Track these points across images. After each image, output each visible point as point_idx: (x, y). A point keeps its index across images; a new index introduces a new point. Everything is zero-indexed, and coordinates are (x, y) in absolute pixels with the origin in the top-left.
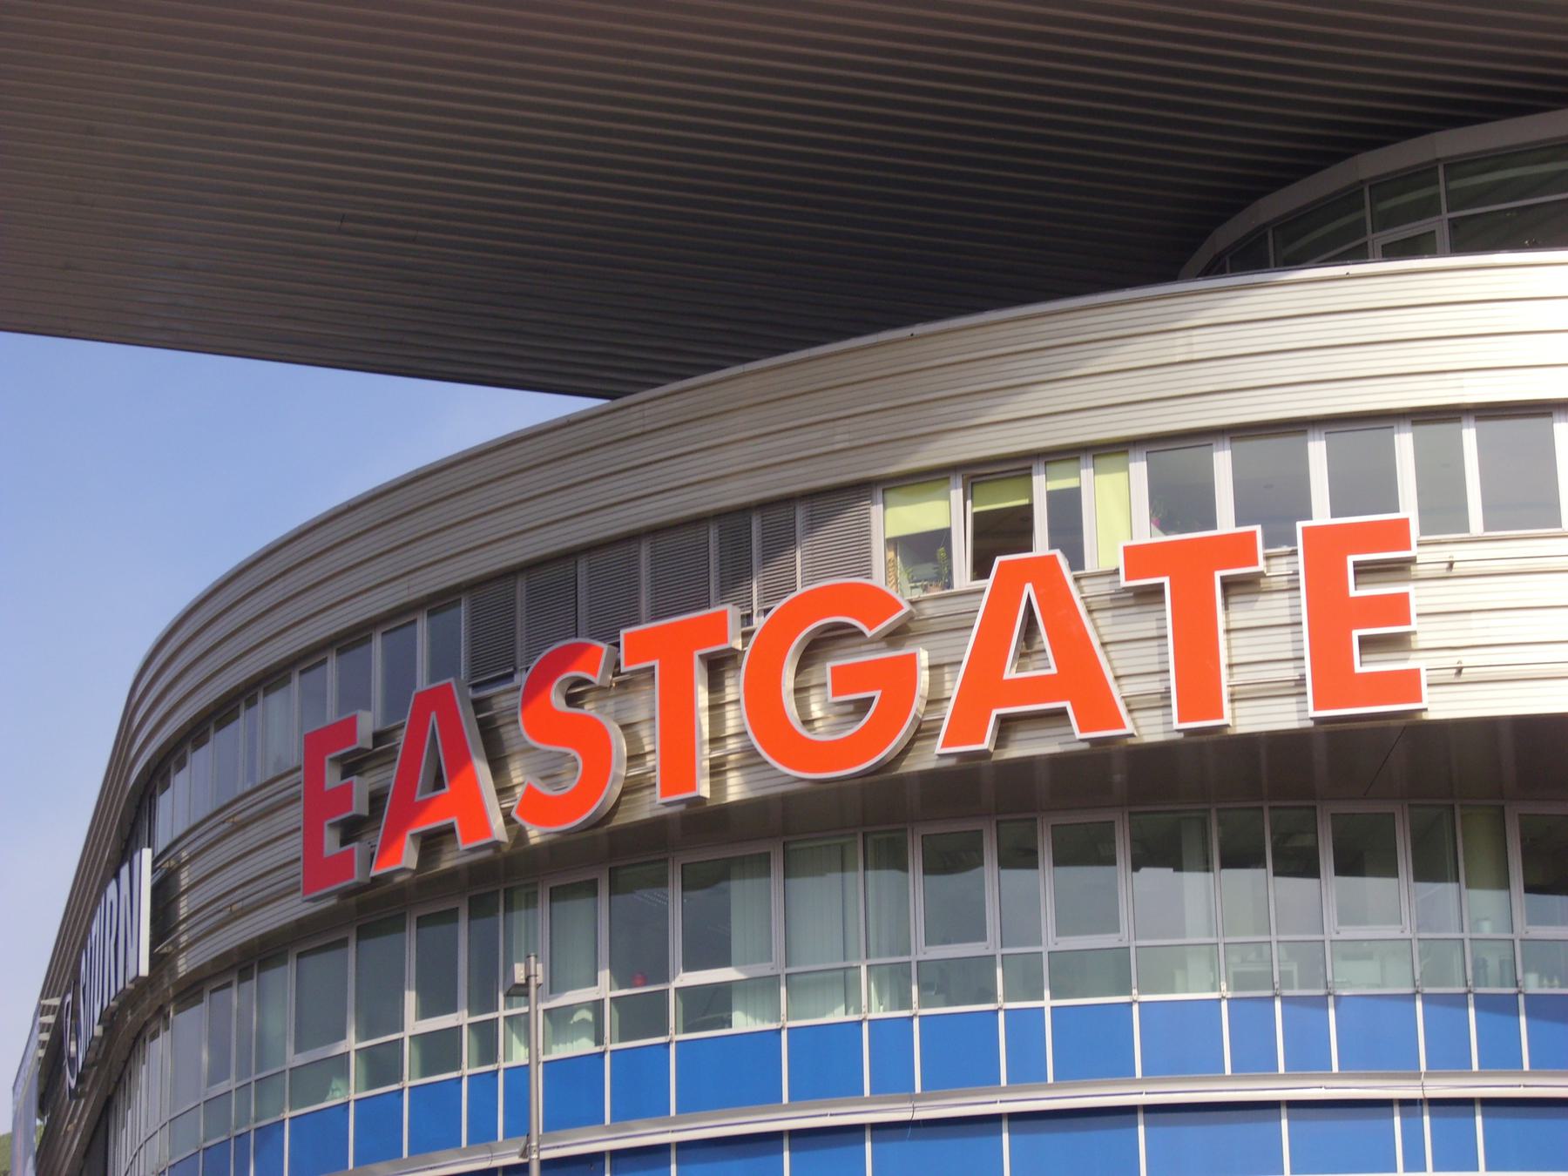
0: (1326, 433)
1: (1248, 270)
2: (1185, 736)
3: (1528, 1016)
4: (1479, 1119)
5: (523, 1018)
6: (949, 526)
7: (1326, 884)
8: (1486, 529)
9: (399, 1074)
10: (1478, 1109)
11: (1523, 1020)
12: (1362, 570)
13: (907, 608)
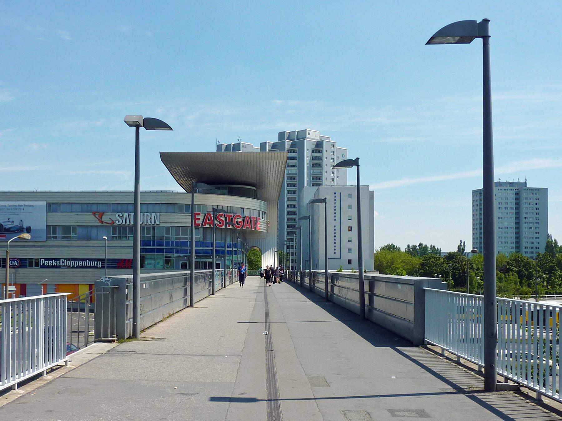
0: (559, 313)
2: (70, 358)
5: (288, 139)
6: (88, 285)
7: (227, 233)
9: (247, 196)
13: (128, 235)
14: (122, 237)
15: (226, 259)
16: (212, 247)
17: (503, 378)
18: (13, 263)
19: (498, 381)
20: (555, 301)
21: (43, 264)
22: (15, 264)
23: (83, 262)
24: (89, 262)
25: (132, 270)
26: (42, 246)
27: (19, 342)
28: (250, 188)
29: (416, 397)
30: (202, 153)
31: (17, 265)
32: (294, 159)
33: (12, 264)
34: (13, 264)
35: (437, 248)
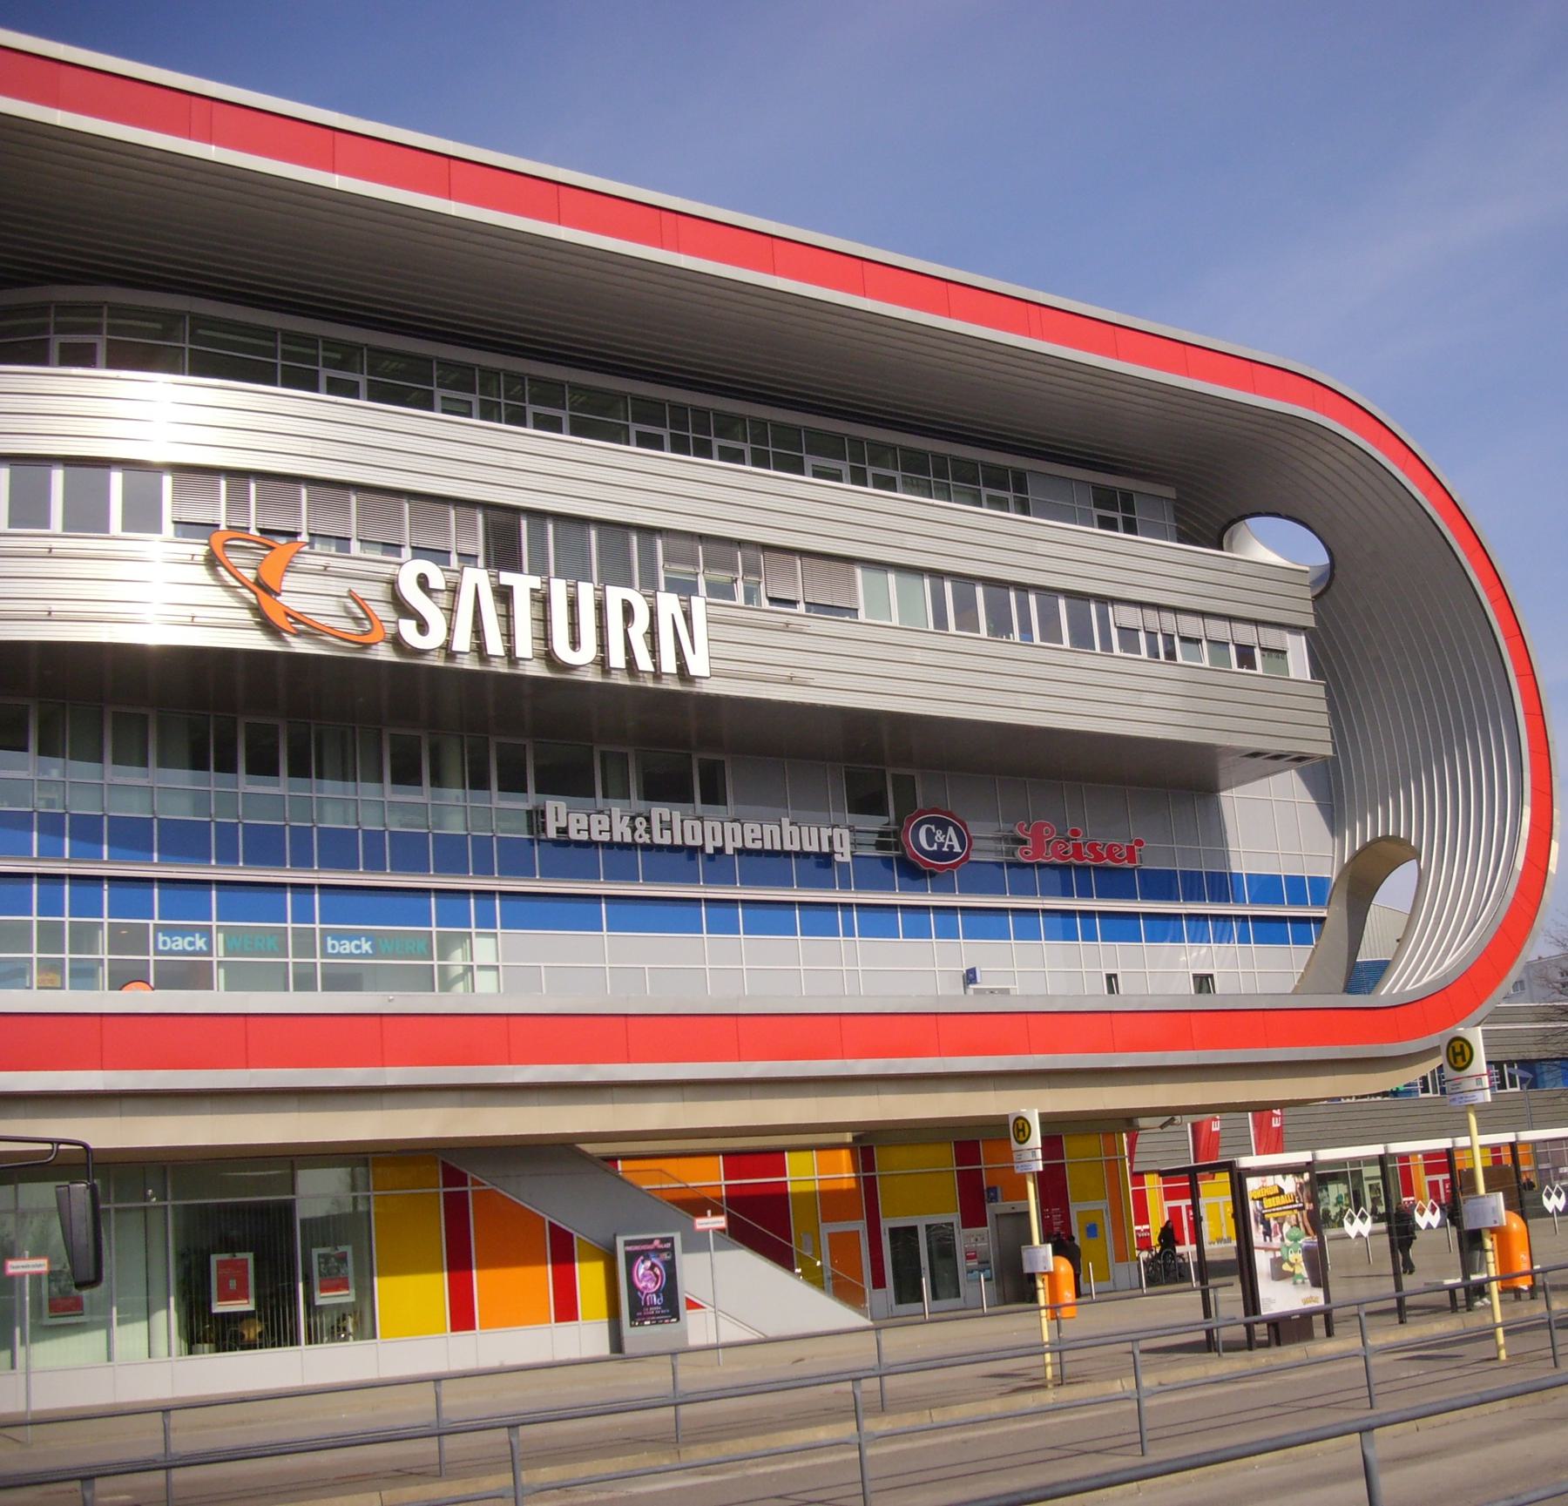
1: (551, 876)
3: (71, 838)
4: (603, 905)
8: (64, 530)
10: (433, 894)
11: (67, 840)
12: (575, 643)
14: (155, 954)
15: (36, 796)
16: (229, 527)
17: (351, 1209)
18: (939, 836)
19: (688, 1300)
20: (1185, 1381)
21: (559, 830)
22: (951, 847)
23: (767, 828)
24: (795, 829)
25: (1486, 1285)
26: (301, 193)
27: (1437, 923)
28: (75, 341)
29: (1476, 1417)
30: (1125, 1110)
31: (959, 854)
32: (1169, 648)
33: (935, 848)
34: (941, 845)
35: (1433, 1214)
